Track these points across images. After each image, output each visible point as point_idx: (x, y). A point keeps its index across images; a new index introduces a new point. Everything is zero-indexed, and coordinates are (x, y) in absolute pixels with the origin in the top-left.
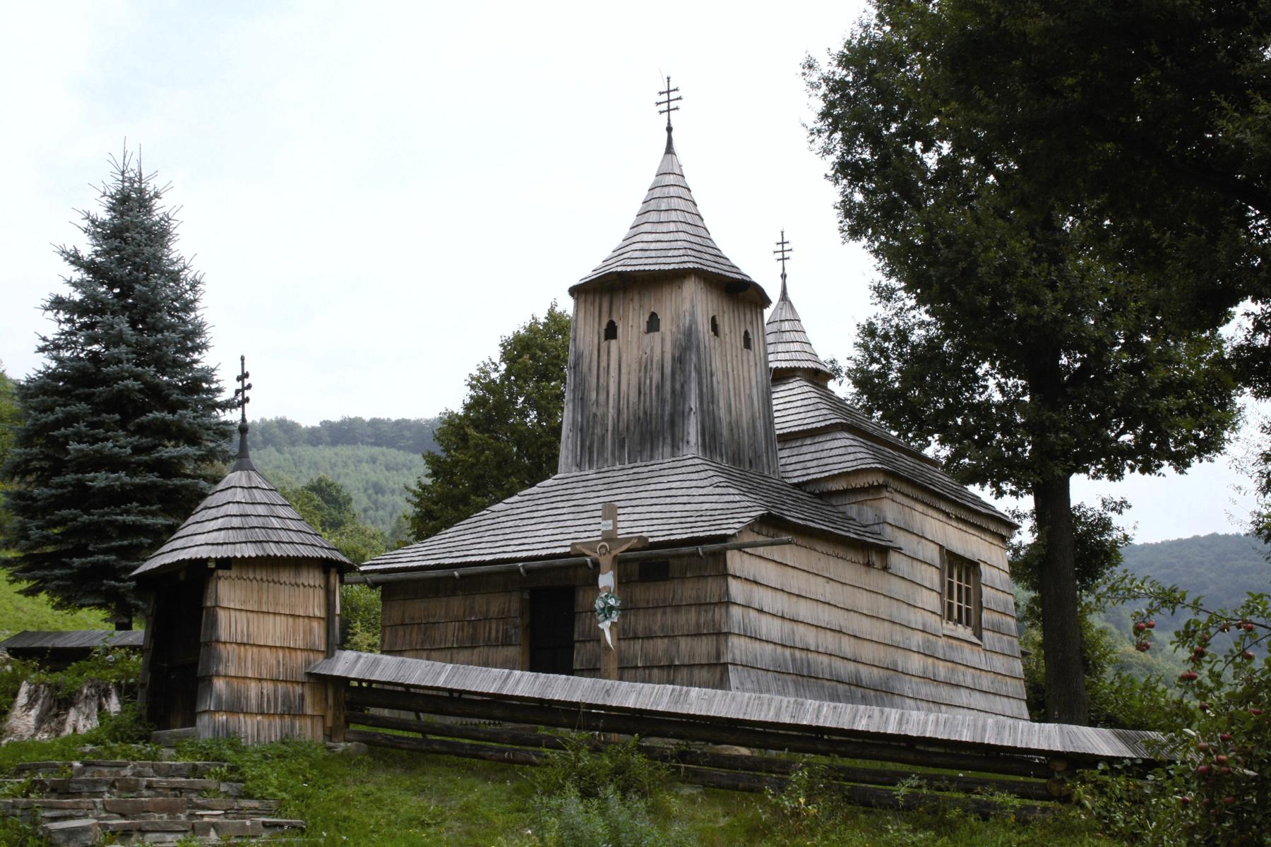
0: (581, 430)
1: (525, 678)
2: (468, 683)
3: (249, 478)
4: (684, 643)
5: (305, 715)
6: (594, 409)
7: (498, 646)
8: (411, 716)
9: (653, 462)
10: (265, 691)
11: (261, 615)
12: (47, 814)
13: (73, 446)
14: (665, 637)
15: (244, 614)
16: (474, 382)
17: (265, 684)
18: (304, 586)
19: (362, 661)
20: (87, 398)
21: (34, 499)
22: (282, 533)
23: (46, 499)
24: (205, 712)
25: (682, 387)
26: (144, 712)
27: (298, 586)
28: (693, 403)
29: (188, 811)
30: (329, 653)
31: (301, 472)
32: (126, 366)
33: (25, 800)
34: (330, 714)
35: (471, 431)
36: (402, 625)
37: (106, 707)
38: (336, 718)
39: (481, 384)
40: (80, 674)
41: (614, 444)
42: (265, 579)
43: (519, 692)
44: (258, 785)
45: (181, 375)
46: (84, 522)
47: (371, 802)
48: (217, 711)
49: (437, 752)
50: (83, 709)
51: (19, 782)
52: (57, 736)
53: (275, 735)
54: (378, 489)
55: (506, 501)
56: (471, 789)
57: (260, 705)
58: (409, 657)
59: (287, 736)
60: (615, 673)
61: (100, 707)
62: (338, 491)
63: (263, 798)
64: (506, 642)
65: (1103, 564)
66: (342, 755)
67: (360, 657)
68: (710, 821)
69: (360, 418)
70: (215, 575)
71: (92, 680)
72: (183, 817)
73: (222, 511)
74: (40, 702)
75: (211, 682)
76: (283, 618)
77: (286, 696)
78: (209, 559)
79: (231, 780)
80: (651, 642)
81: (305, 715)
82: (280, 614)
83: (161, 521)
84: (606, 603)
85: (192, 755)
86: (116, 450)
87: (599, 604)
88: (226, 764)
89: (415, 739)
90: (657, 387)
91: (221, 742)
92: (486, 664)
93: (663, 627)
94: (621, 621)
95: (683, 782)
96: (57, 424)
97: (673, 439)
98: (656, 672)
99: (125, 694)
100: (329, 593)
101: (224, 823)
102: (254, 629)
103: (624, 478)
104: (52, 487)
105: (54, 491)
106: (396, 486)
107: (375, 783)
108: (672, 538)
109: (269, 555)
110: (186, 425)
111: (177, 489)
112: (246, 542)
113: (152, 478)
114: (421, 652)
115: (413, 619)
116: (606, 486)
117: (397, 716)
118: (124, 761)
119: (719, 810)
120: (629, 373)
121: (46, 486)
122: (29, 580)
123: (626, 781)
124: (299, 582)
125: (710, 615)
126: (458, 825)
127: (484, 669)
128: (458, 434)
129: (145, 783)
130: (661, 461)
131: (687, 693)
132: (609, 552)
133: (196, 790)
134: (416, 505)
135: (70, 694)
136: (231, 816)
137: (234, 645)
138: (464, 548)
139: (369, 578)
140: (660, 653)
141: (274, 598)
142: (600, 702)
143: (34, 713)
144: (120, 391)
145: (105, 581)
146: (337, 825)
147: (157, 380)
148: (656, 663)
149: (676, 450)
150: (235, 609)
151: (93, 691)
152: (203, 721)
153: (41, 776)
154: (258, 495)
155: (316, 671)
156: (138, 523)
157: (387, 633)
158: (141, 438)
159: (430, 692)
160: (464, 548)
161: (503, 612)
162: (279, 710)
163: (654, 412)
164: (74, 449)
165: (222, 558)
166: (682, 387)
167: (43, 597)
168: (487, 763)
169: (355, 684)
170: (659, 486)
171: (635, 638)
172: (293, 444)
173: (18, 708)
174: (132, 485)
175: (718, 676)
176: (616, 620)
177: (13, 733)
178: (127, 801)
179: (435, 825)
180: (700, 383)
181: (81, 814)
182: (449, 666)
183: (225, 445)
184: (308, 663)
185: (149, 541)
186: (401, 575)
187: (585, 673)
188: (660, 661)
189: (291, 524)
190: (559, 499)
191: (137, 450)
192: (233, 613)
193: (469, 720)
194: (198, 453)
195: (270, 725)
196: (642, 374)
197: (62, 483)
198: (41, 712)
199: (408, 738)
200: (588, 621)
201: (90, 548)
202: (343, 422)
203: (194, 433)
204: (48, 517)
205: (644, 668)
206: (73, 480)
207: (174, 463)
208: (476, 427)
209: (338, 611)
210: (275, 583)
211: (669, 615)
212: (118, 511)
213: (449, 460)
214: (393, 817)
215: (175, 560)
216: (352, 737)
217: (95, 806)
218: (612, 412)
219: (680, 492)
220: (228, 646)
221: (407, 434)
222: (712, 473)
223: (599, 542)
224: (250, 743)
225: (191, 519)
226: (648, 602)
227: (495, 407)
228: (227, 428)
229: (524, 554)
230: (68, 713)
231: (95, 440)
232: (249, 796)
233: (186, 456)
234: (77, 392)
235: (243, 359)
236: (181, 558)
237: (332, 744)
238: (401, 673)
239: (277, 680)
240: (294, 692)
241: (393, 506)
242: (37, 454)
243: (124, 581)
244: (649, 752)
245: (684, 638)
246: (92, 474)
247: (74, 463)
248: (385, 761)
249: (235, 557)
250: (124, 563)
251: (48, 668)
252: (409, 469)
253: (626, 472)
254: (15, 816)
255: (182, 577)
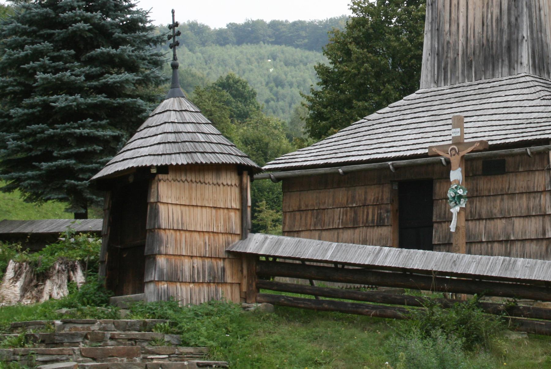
0: (438, 54)
1: (392, 253)
2: (349, 257)
3: (180, 103)
4: (518, 223)
5: (226, 283)
6: (447, 38)
7: (374, 226)
8: (306, 282)
9: (494, 79)
10: (195, 266)
11: (192, 208)
12: (40, 358)
13: (40, 76)
14: (503, 218)
15: (178, 207)
16: (356, 7)
17: (195, 260)
18: (224, 185)
19: (268, 241)
20: (49, 38)
21: (10, 117)
22: (206, 145)
23: (20, 116)
24: (151, 282)
25: (516, 20)
26: (104, 283)
27: (219, 185)
28: (525, 32)
29: (142, 356)
30: (243, 236)
31: (210, 68)
32: (78, 12)
33: (23, 349)
34: (245, 282)
35: (353, 47)
36: (299, 211)
37: (74, 279)
38: (249, 285)
39: (361, 7)
40: (52, 254)
41: (463, 65)
42: (194, 180)
43: (387, 263)
44: (192, 336)
45: (121, 16)
46: (50, 134)
47: (277, 347)
48: (161, 280)
49: (326, 310)
50: (57, 281)
51: (16, 336)
52: (38, 301)
53: (204, 298)
54: (279, 83)
55: (379, 111)
56: (352, 337)
57: (192, 276)
58: (303, 237)
59: (213, 299)
60: (463, 247)
61: (69, 279)
62: (244, 87)
63: (196, 345)
64: (380, 224)
65: (300, 321)
66: (254, 313)
67: (266, 238)
68: (532, 359)
69: (262, 21)
70: (156, 178)
71: (62, 259)
72: (138, 360)
73: (160, 129)
74: (23, 275)
75: (154, 259)
76: (208, 210)
77: (211, 268)
78: (151, 167)
79: (172, 333)
80: (492, 222)
81: (226, 283)
82: (206, 207)
83: (109, 133)
84: (456, 193)
85: (143, 314)
86: (73, 78)
87: (451, 194)
88: (168, 321)
89: (309, 300)
90: (497, 20)
91: (163, 304)
92: (365, 242)
93: (501, 211)
94: (469, 206)
95: (513, 330)
96: (26, 59)
97: (510, 61)
98: (496, 245)
99: (89, 269)
100: (242, 190)
101: (168, 364)
102: (186, 219)
103: (472, 92)
104: (25, 108)
105: (26, 111)
106: (294, 80)
107: (280, 334)
108: (507, 141)
109: (196, 163)
110: (127, 57)
111: (121, 107)
112: (179, 153)
113: (101, 98)
114: (314, 232)
115: (307, 206)
116: (457, 100)
117: (295, 282)
118: (92, 319)
119: (540, 350)
120: (474, 9)
121: (20, 107)
122: (7, 179)
123: (468, 329)
124: (220, 182)
125: (538, 200)
126: (342, 363)
127: (361, 246)
128: (343, 49)
129: (109, 336)
130: (500, 79)
131: (515, 262)
132: (458, 154)
133: (147, 340)
134: (311, 108)
135: (46, 269)
136: (173, 359)
137: (172, 231)
138: (346, 150)
139: (273, 175)
140: (499, 231)
141: (201, 195)
142: (449, 270)
143: (19, 284)
144: (74, 32)
145: (67, 181)
146: (252, 365)
147: (103, 22)
148: (496, 239)
149: (512, 70)
150: (172, 204)
151: (64, 267)
152: (150, 289)
153: (31, 331)
154: (188, 117)
155: (234, 250)
156: (91, 134)
157: (288, 217)
158: (91, 67)
159: (322, 264)
160: (346, 150)
161: (378, 200)
162: (207, 280)
163: (495, 40)
164: (41, 78)
165: (161, 165)
166: (516, 20)
167: (17, 193)
168: (364, 317)
169: (264, 259)
170: (498, 99)
171: (480, 219)
172: (203, 44)
173: (7, 281)
174: (85, 104)
175: (544, 248)
176: (464, 206)
177: (4, 299)
178: (97, 349)
179: (325, 364)
180: (530, 17)
181: (64, 358)
182: (335, 245)
183: (157, 72)
184: (228, 244)
185: (101, 148)
186: (297, 172)
187: (442, 247)
188: (499, 237)
189: (213, 138)
190: (421, 109)
191: (89, 77)
192: (170, 206)
193: (352, 285)
194: (136, 78)
195: (200, 290)
196: (485, 9)
197: (31, 104)
198: (24, 283)
199: (305, 300)
200: (443, 206)
201: (55, 154)
202: (247, 25)
203: (134, 62)
204: (21, 131)
205: (488, 242)
206: (41, 101)
207: (117, 86)
208: (357, 44)
209: (249, 204)
210: (202, 183)
211: (506, 201)
212: (76, 125)
213: (336, 70)
214: (294, 358)
215: (126, 167)
216: (262, 299)
217: (75, 353)
218: (462, 40)
219: (514, 104)
220: (167, 231)
221: (303, 34)
222: (539, 88)
223: (450, 145)
224: (185, 304)
225: (136, 136)
226: (489, 191)
227: (372, 26)
228: (158, 58)
229: (393, 155)
230: (45, 284)
231: (56, 70)
232: (186, 344)
233: (127, 81)
234: (42, 32)
235: (173, 12)
236: (131, 166)
237: (247, 305)
238: (299, 250)
239: (205, 257)
240: (217, 266)
241: (292, 98)
242: (12, 82)
243: (82, 180)
244: (485, 307)
245: (518, 219)
246: (55, 97)
247: (40, 88)
248: (287, 317)
249: (171, 165)
250: (81, 166)
251: (28, 249)
252: (305, 64)
253: (473, 88)
254: (17, 361)
255: (131, 179)
